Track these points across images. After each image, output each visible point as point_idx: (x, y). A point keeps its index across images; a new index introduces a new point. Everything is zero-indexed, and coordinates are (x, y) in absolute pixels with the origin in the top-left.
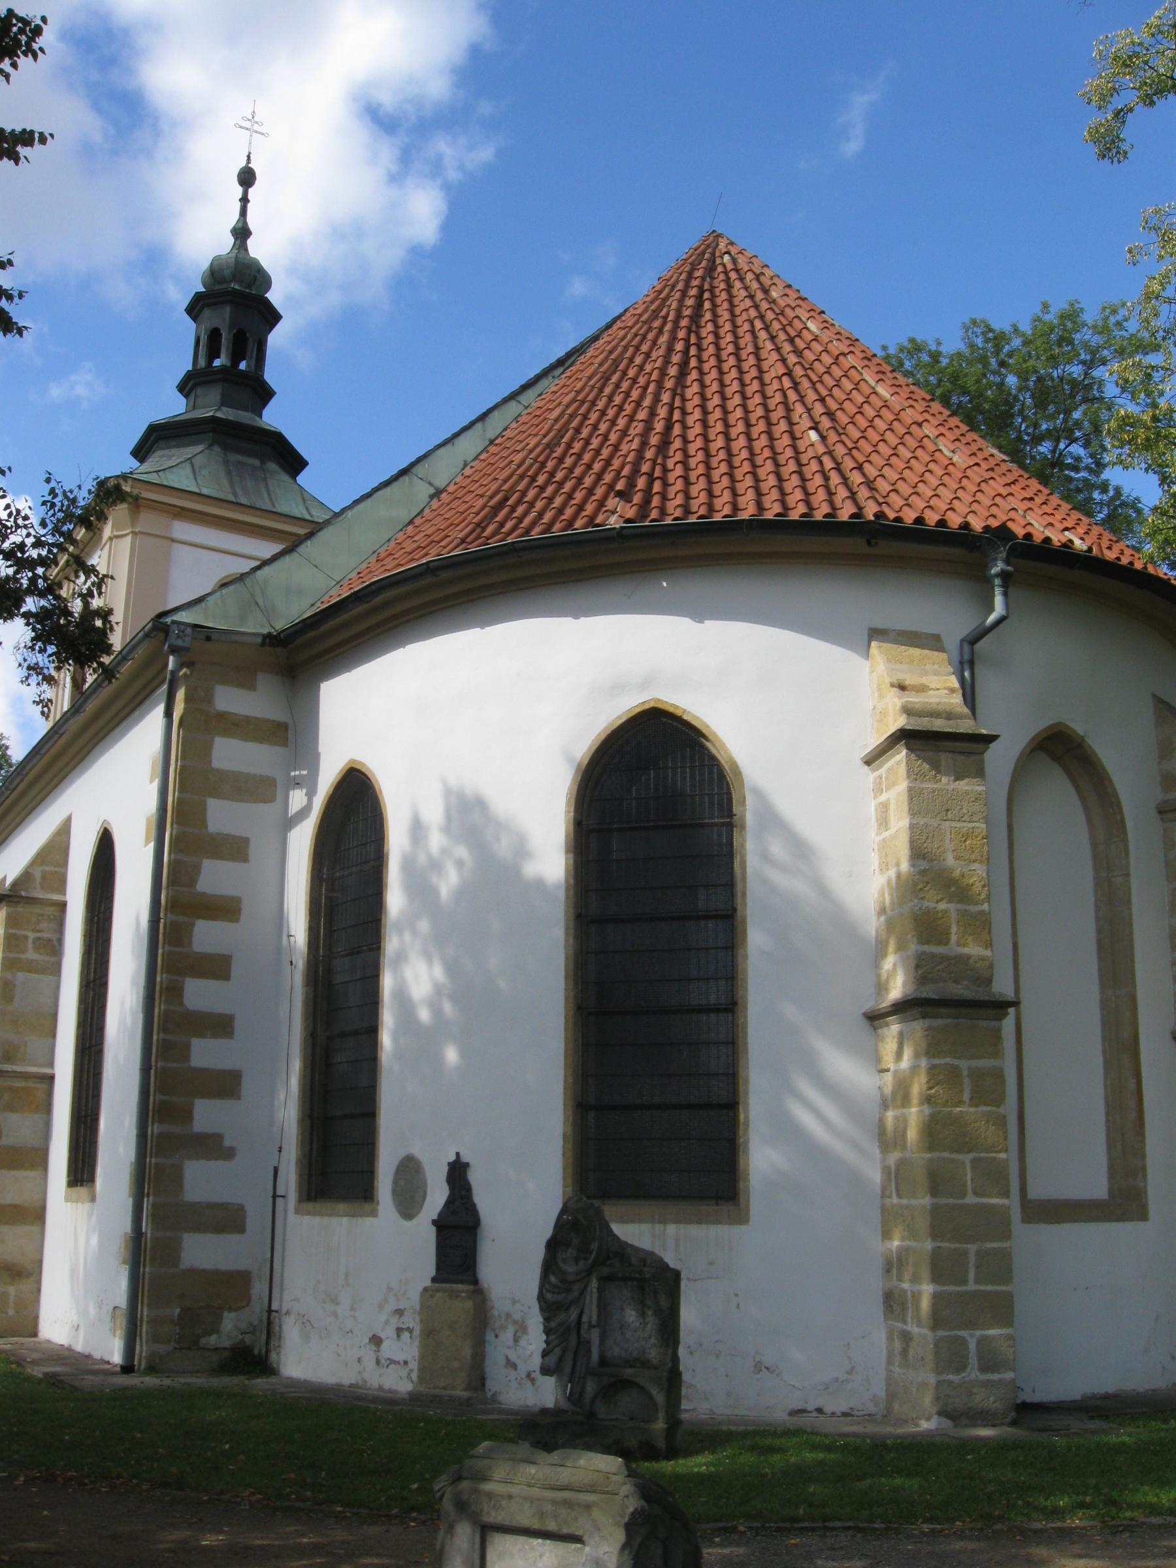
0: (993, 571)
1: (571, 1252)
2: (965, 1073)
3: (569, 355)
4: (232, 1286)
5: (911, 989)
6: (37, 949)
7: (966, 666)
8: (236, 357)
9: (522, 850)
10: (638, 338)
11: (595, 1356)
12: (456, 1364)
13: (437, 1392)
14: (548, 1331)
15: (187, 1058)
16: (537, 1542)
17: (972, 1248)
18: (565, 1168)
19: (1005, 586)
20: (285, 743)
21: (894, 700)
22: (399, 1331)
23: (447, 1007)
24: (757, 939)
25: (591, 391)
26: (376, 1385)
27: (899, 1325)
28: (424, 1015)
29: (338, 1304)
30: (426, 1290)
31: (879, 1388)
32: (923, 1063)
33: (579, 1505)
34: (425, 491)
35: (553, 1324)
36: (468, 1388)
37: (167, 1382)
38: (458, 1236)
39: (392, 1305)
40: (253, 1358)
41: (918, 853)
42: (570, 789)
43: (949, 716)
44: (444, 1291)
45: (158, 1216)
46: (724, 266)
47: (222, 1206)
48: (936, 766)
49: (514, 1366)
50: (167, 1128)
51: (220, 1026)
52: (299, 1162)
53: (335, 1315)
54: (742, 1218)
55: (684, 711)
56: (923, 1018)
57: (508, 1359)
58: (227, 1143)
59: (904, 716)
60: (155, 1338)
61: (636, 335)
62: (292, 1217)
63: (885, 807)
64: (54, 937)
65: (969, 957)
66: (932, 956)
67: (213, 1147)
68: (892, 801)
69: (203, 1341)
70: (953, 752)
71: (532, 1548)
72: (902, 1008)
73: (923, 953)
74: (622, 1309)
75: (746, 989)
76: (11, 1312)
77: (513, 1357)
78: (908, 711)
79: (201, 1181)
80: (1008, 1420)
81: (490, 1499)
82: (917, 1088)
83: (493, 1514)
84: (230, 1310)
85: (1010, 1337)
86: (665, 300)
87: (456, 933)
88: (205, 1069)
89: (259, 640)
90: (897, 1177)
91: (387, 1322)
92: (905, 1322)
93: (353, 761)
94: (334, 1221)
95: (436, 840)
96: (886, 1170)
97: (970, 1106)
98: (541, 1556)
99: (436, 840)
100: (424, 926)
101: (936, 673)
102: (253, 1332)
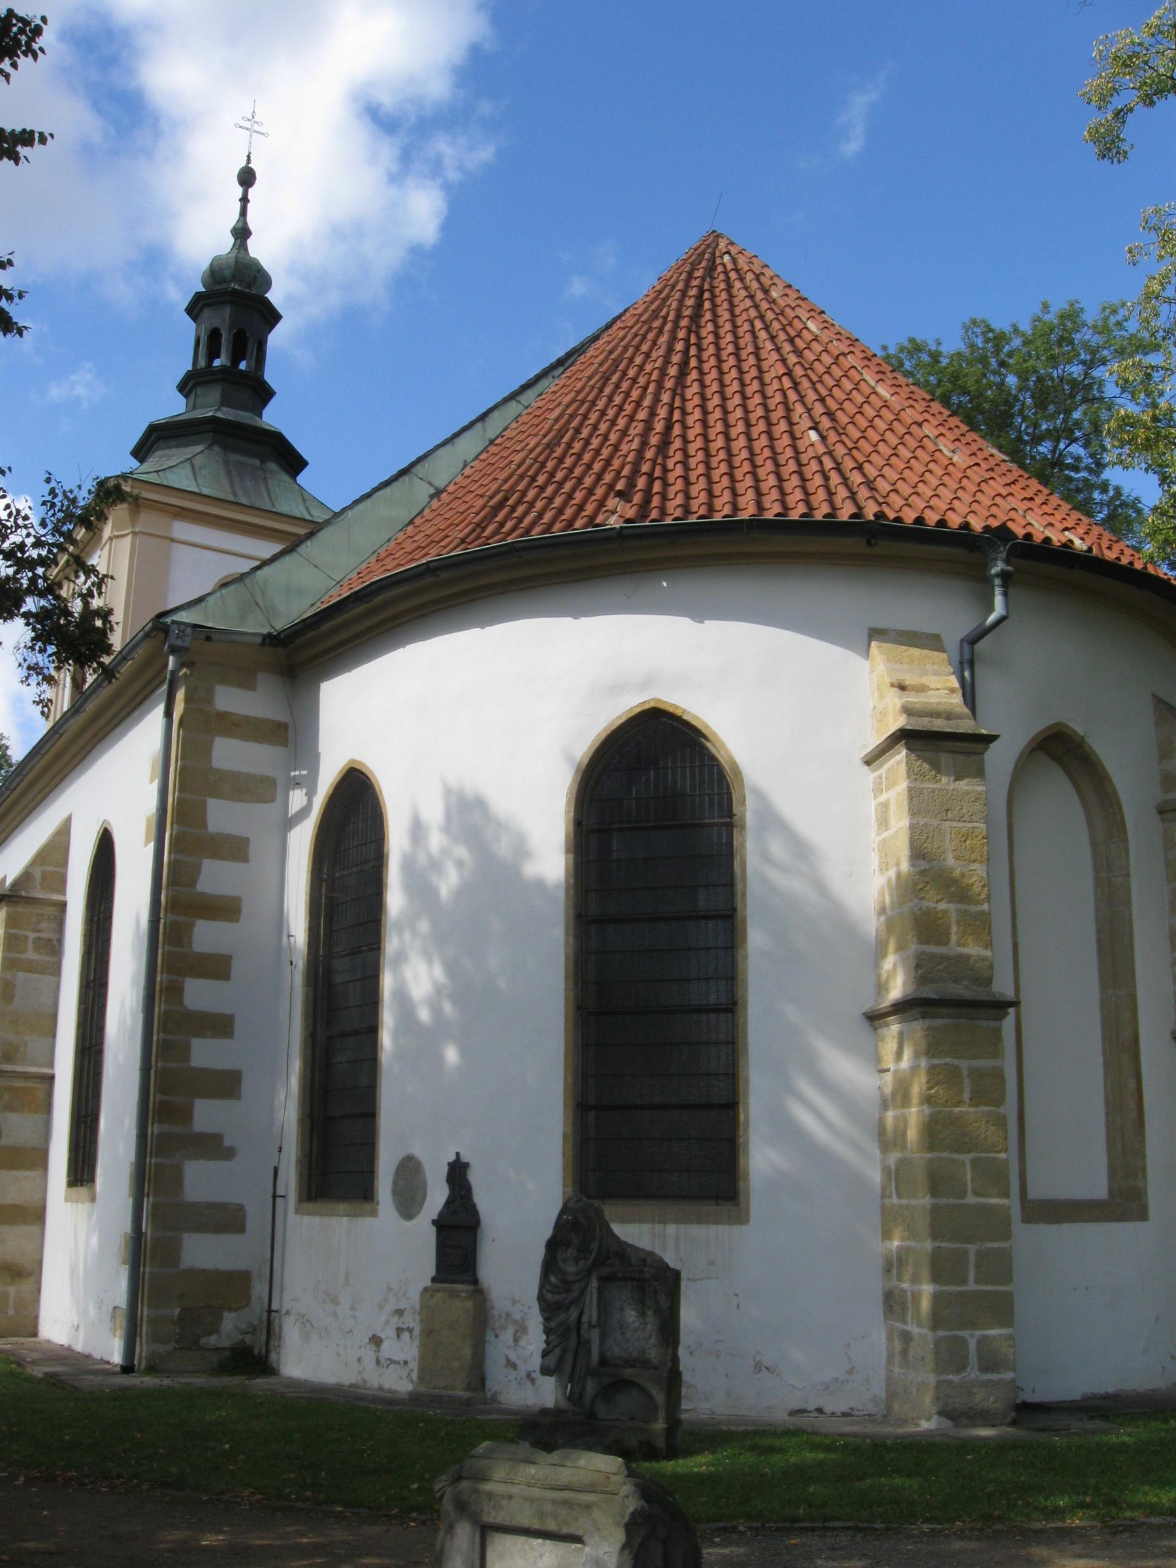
0: (993, 571)
1: (571, 1252)
2: (965, 1073)
3: (569, 355)
4: (232, 1286)
5: (911, 989)
6: (37, 949)
7: (966, 666)
8: (236, 357)
9: (522, 850)
10: (638, 338)
11: (595, 1356)
12: (456, 1364)
13: (437, 1392)
14: (548, 1331)
15: (187, 1058)
16: (537, 1542)
17: (972, 1248)
18: (565, 1168)
19: (1005, 586)
20: (285, 743)
21: (894, 700)
22: (399, 1331)
23: (447, 1007)
24: (757, 939)
25: (591, 391)
26: (376, 1385)
27: (899, 1325)
28: (424, 1015)
29: (338, 1304)
30: (426, 1290)
31: (879, 1388)
32: (923, 1063)
33: (579, 1505)
34: (425, 491)
35: (553, 1324)
36: (468, 1388)
37: (167, 1382)
38: (458, 1236)
39: (392, 1305)
40: (253, 1358)
41: (918, 853)
42: (570, 789)
43: (949, 716)
44: (444, 1291)
45: (158, 1216)
46: (724, 266)
47: (222, 1206)
48: (936, 766)
49: (514, 1366)
50: (167, 1128)
51: (220, 1026)
52: (299, 1162)
53: (335, 1315)
54: (742, 1218)
55: (684, 711)
56: (923, 1018)
57: (508, 1359)
58: (227, 1143)
59: (904, 716)
60: (155, 1338)
61: (636, 335)
62: (292, 1217)
63: (885, 807)
64: (54, 937)
65: (969, 957)
66: (932, 956)
67: (213, 1147)
68: (892, 801)
69: (203, 1341)
70: (953, 752)
71: (532, 1548)
72: (902, 1008)
73: (923, 953)
74: (622, 1309)
75: (746, 989)
76: (11, 1312)
77: (513, 1357)
78: (908, 711)
79: (201, 1181)
80: (1008, 1420)
81: (490, 1499)
82: (917, 1088)
83: (493, 1514)
84: (230, 1310)
85: (1010, 1337)
86: (665, 300)
87: (456, 933)
88: (205, 1069)
89: (259, 640)
90: (897, 1177)
91: (387, 1322)
92: (905, 1322)
93: (353, 761)
94: (334, 1221)
95: (436, 840)
96: (886, 1170)
97: (970, 1106)
98: (541, 1556)
99: (436, 840)
100: (424, 926)
101: (936, 673)
102: (253, 1332)
